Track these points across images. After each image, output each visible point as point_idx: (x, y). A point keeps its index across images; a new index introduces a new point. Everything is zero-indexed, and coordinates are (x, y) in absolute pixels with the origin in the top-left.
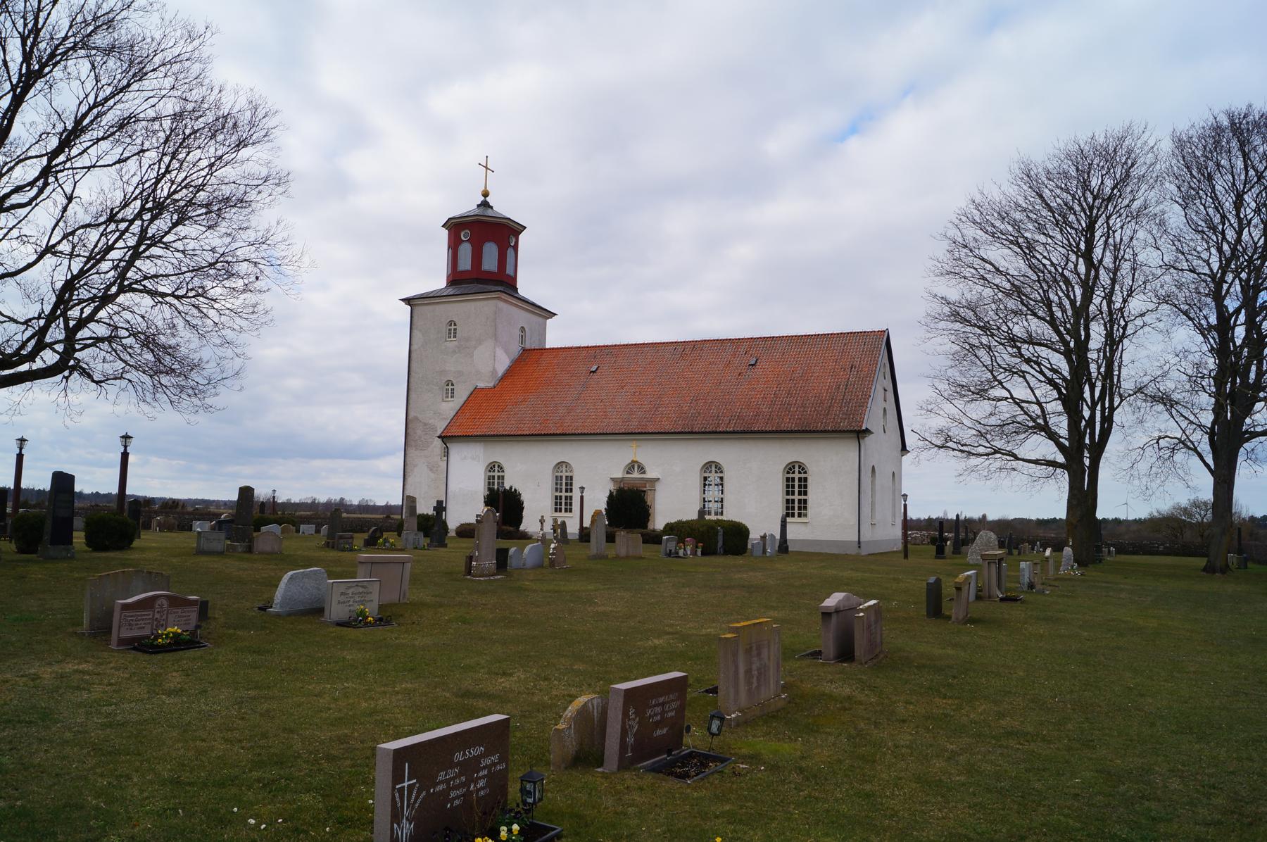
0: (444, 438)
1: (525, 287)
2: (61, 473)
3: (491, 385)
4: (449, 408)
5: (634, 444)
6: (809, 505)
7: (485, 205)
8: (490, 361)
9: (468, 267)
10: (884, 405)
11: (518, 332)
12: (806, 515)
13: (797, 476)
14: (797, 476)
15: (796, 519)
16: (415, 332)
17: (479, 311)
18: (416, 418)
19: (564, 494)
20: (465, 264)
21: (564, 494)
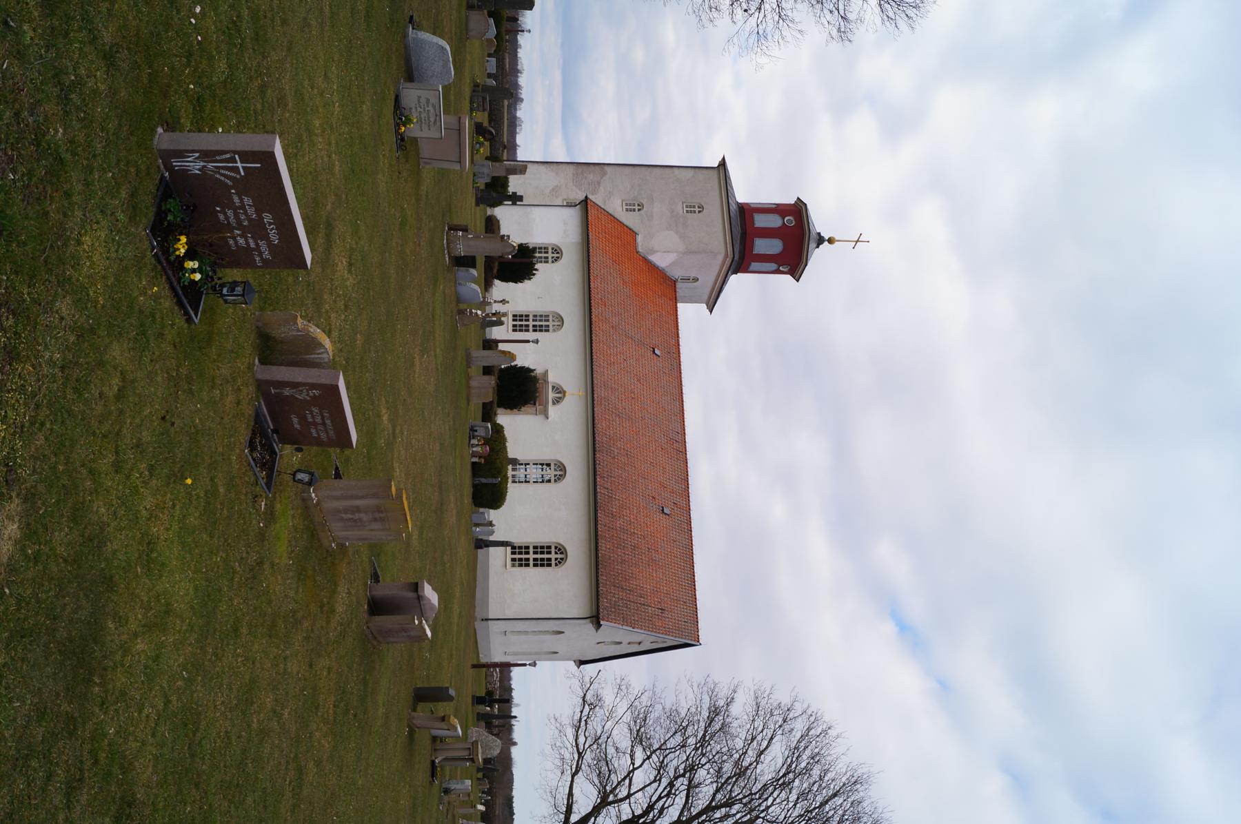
0: (585, 202)
1: (737, 282)
3: (640, 249)
4: (616, 207)
5: (582, 393)
6: (524, 569)
7: (820, 240)
8: (663, 248)
10: (625, 642)
11: (693, 275)
12: (513, 566)
13: (553, 556)
14: (553, 556)
15: (509, 556)
16: (691, 172)
17: (714, 235)
18: (605, 174)
19: (531, 323)
20: (761, 221)
21: (531, 323)
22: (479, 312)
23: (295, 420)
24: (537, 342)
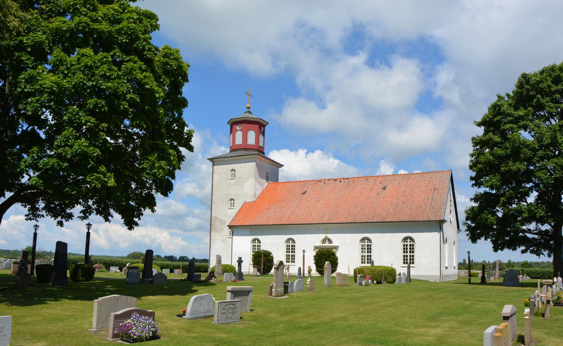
0: (230, 227)
2: (61, 242)
3: (253, 200)
4: (232, 213)
9: (241, 143)
12: (294, 262)
18: (216, 217)
20: (239, 140)
21: (291, 254)
22: (308, 280)
23: (20, 295)
24: (304, 251)
